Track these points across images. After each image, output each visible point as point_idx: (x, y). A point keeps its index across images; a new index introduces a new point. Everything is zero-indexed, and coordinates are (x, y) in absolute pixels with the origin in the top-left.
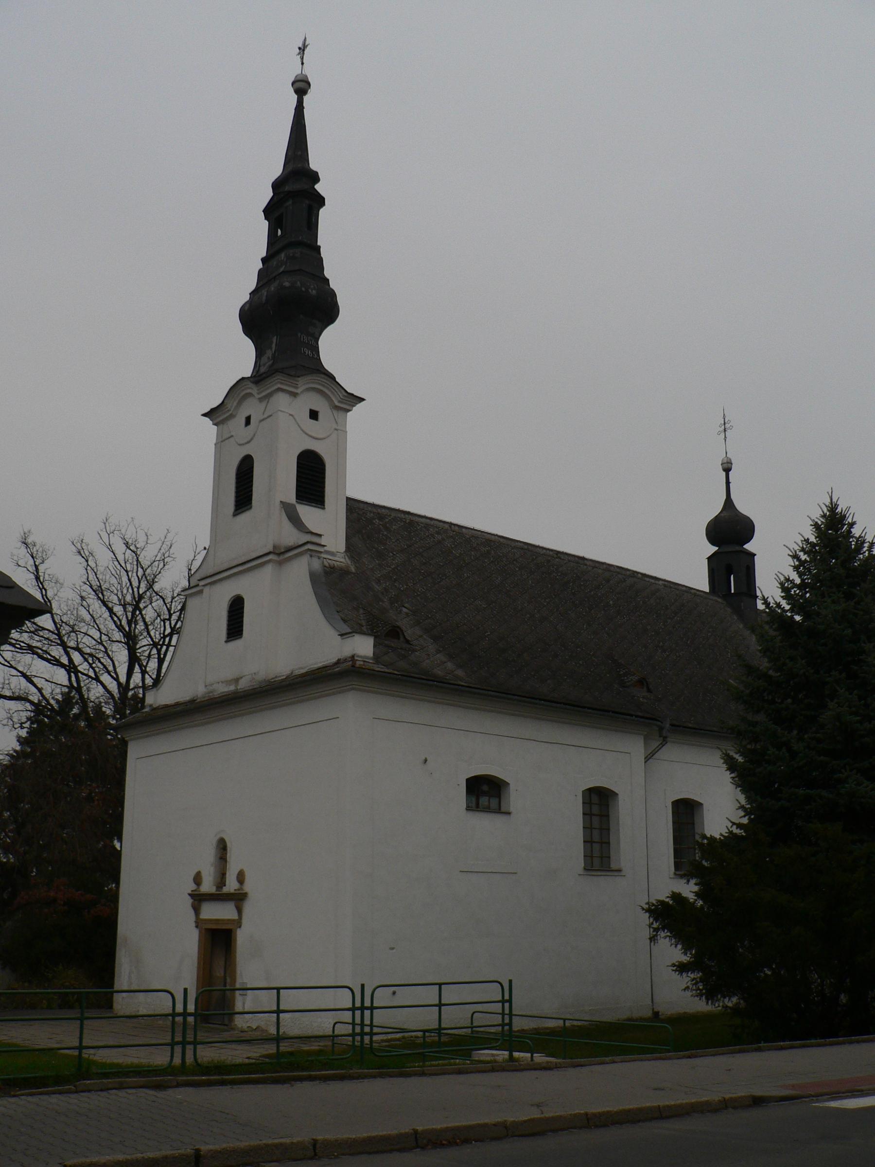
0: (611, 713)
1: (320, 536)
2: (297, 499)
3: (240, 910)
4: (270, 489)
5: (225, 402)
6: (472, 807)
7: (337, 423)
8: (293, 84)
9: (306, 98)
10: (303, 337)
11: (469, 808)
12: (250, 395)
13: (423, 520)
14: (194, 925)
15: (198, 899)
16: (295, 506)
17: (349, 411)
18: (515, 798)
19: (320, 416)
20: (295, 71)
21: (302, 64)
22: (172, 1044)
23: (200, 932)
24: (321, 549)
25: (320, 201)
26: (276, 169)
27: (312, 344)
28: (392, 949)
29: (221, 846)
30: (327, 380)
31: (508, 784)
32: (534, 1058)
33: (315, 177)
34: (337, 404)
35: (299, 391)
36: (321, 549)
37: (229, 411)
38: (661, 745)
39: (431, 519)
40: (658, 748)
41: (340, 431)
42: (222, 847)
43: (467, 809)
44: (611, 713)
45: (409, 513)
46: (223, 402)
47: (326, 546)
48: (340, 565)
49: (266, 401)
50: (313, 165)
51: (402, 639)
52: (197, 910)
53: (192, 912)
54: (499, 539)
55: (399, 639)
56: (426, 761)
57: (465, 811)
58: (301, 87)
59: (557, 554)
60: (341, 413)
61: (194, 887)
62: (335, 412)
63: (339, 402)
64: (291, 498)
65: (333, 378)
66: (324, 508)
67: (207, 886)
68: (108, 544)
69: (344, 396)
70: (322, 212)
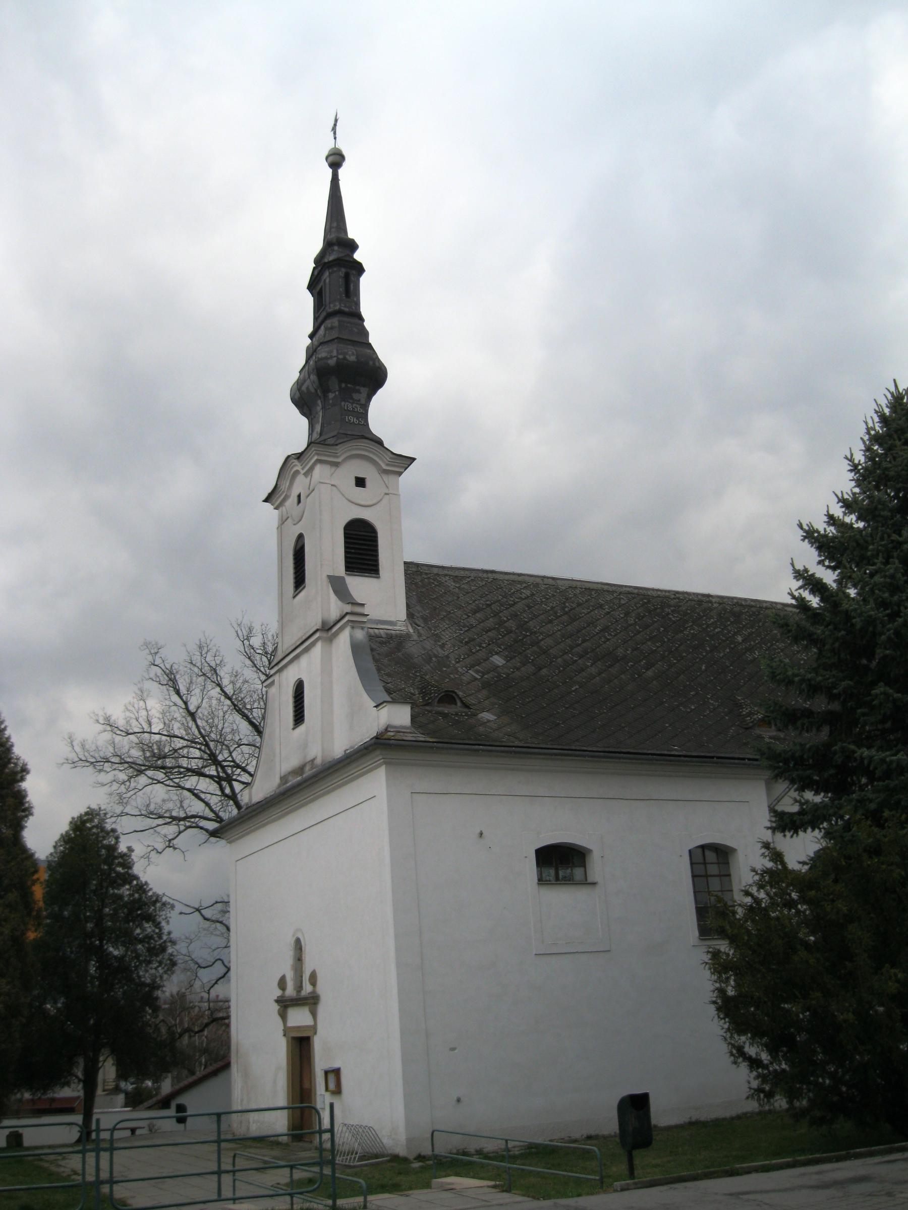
0: (715, 759)
1: (363, 605)
2: (346, 571)
3: (314, 1014)
4: (782, 626)
5: (278, 483)
6: (550, 881)
7: (387, 487)
8: (327, 159)
9: (341, 172)
10: (347, 405)
11: (541, 881)
12: (297, 472)
13: (507, 577)
14: (282, 1033)
15: (285, 1004)
16: (343, 579)
17: (400, 474)
18: (597, 868)
19: (368, 483)
20: (329, 145)
21: (335, 138)
22: (219, 1173)
23: (288, 1042)
24: (364, 619)
25: (359, 269)
26: (317, 244)
27: (357, 411)
28: (453, 1049)
29: (298, 947)
30: (369, 444)
31: (590, 851)
32: (368, 1204)
33: (352, 246)
34: (385, 467)
35: (339, 460)
36: (364, 619)
37: (283, 492)
38: (788, 789)
39: (520, 575)
40: (785, 793)
41: (391, 494)
42: (298, 946)
43: (538, 884)
44: (715, 759)
45: (493, 572)
46: (276, 484)
47: (368, 615)
48: (399, 634)
49: (310, 476)
50: (351, 235)
51: (459, 704)
52: (283, 1015)
53: (279, 1020)
54: (603, 586)
55: (456, 704)
56: (481, 834)
57: (536, 886)
58: (336, 160)
59: (675, 595)
60: (392, 478)
61: (279, 993)
62: (385, 477)
63: (387, 465)
64: (339, 568)
65: (379, 442)
66: (378, 577)
67: (290, 991)
68: (243, 652)
69: (391, 458)
70: (364, 280)
